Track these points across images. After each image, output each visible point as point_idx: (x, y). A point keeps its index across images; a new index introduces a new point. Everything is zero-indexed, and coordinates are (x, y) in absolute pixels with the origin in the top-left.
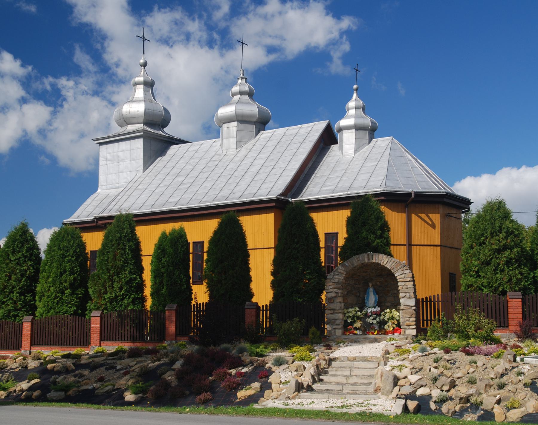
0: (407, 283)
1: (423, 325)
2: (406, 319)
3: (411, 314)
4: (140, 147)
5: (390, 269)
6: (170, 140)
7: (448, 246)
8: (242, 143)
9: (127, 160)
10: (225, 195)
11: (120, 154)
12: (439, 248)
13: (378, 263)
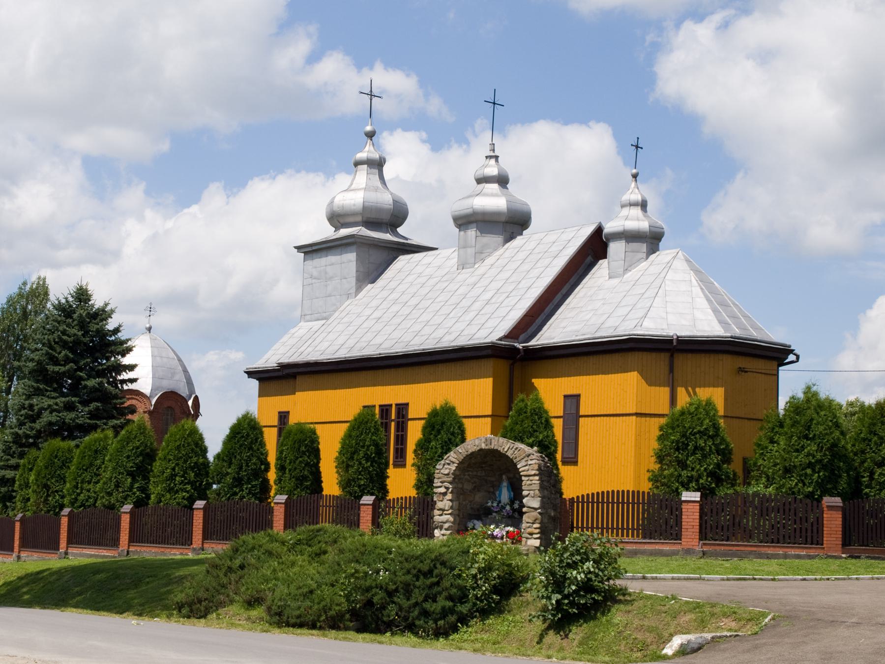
0: (531, 478)
2: (528, 525)
3: (534, 519)
4: (353, 260)
6: (400, 247)
8: (483, 256)
9: (336, 278)
10: (438, 337)
11: (329, 269)
13: (497, 450)
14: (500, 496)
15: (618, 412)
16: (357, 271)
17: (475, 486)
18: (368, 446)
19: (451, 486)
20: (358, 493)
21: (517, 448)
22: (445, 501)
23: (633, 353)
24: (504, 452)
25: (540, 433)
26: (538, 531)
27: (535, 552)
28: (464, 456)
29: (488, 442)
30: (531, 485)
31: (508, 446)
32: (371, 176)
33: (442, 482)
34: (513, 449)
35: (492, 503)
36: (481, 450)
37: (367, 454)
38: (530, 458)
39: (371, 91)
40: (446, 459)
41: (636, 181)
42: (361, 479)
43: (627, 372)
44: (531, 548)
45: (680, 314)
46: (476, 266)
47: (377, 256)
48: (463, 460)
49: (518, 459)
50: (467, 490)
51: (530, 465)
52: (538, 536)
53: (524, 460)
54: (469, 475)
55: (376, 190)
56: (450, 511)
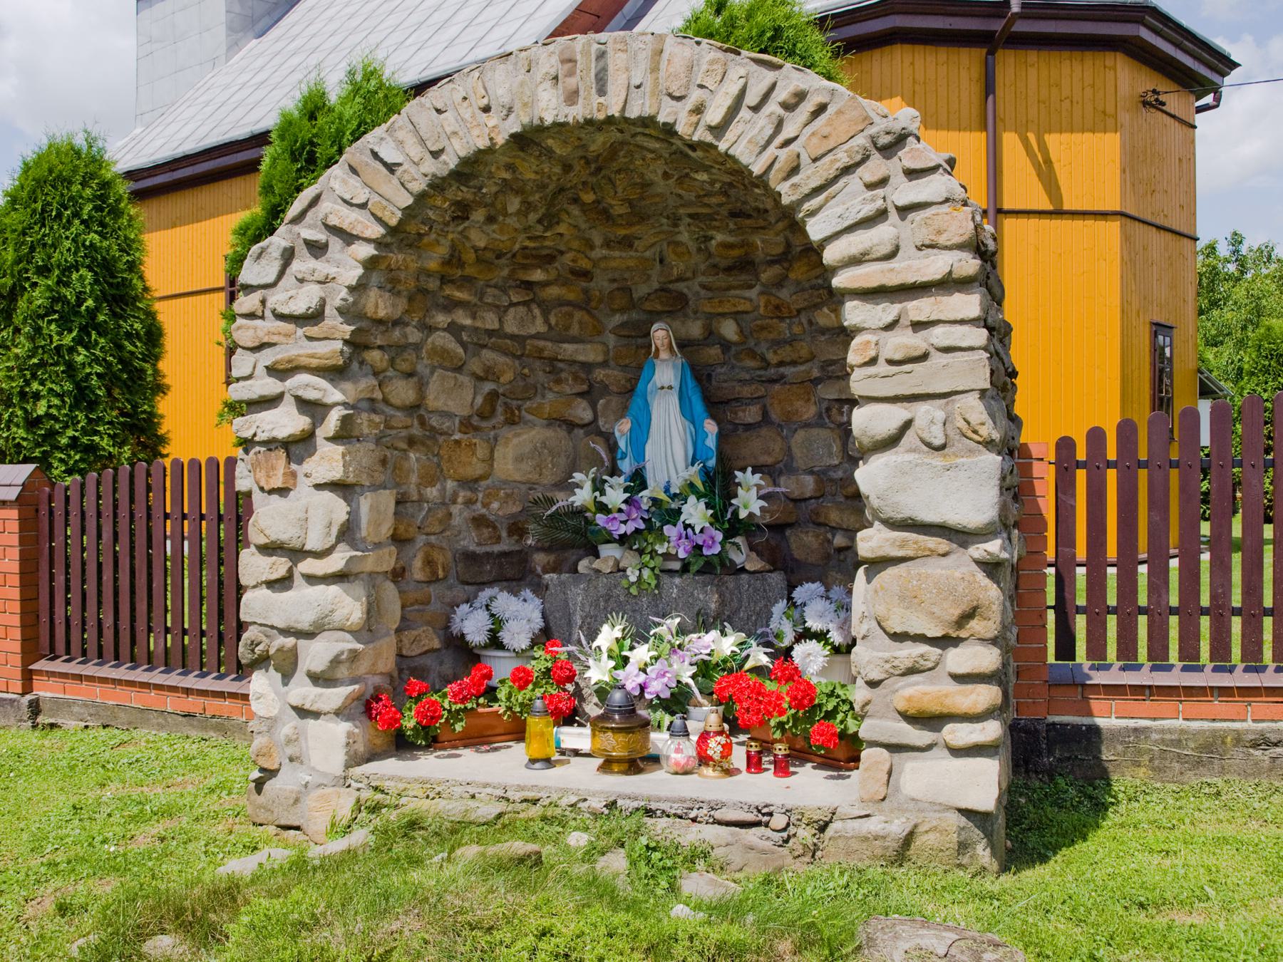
0: (920, 308)
1: (1066, 648)
2: (909, 653)
3: (956, 612)
5: (757, 169)
7: (1149, 218)
12: (1114, 226)
17: (493, 397)
18: (67, 270)
21: (801, 96)
22: (303, 493)
23: (887, 49)
24: (701, 135)
26: (987, 695)
28: (419, 186)
30: (924, 357)
31: (733, 88)
33: (279, 372)
34: (773, 107)
35: (599, 486)
40: (298, 219)
44: (932, 819)
49: (810, 177)
50: (448, 415)
51: (904, 211)
53: (853, 183)
54: (454, 329)
56: (336, 562)
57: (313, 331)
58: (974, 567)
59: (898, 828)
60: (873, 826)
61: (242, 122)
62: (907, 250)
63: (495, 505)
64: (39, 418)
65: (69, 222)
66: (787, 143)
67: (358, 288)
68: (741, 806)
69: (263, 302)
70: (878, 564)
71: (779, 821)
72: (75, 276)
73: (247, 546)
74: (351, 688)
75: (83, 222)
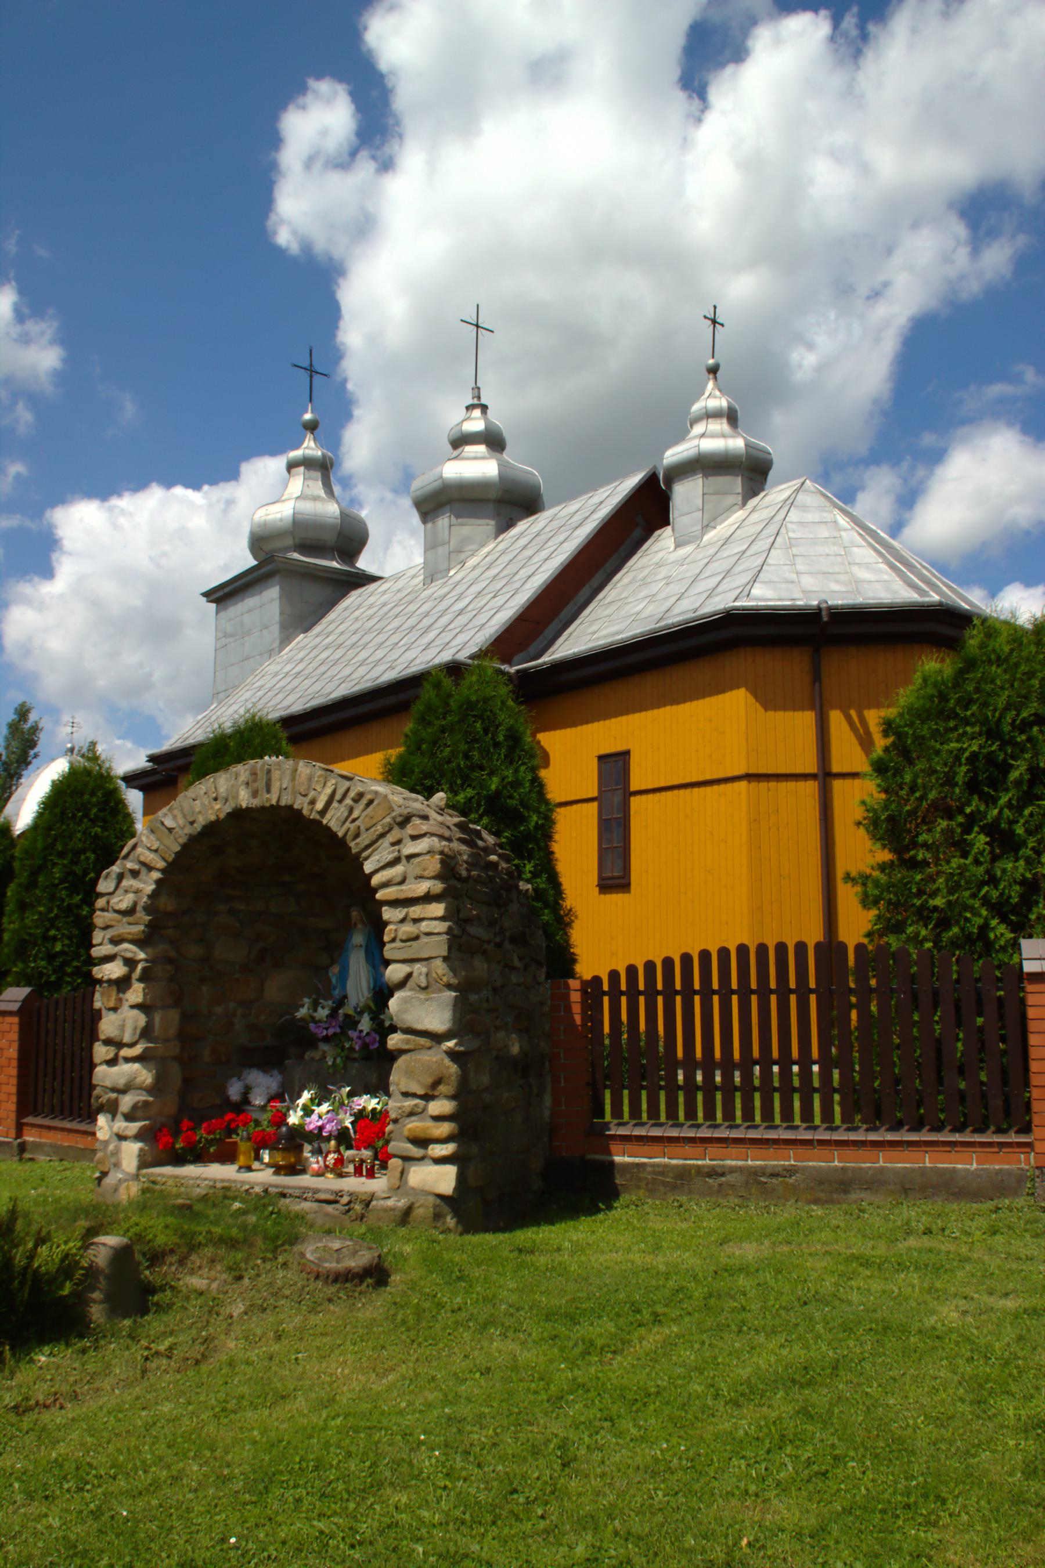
0: (416, 911)
5: (340, 834)
8: (463, 556)
11: (246, 619)
13: (290, 808)
14: (343, 977)
15: (708, 777)
16: (281, 614)
18: (77, 853)
19: (142, 955)
20: (49, 976)
21: (360, 795)
25: (492, 773)
26: (445, 1129)
27: (437, 1216)
29: (261, 784)
30: (417, 938)
31: (328, 791)
32: (310, 483)
34: (348, 801)
35: (315, 1006)
36: (238, 815)
37: (73, 873)
38: (410, 830)
39: (311, 377)
41: (715, 378)
42: (55, 939)
43: (723, 691)
44: (422, 1200)
45: (824, 573)
46: (452, 573)
47: (314, 593)
48: (178, 854)
49: (365, 839)
51: (410, 857)
52: (448, 1149)
55: (316, 498)
56: (137, 1050)
57: (131, 919)
58: (444, 1055)
59: (402, 1203)
60: (390, 1203)
61: (279, 707)
62: (410, 879)
63: (263, 1017)
64: (57, 953)
65: (81, 821)
66: (354, 820)
67: (153, 896)
68: (326, 1191)
69: (108, 902)
70: (402, 1052)
71: (345, 1199)
72: (83, 857)
73: (98, 1040)
74: (143, 1123)
75: (91, 820)
